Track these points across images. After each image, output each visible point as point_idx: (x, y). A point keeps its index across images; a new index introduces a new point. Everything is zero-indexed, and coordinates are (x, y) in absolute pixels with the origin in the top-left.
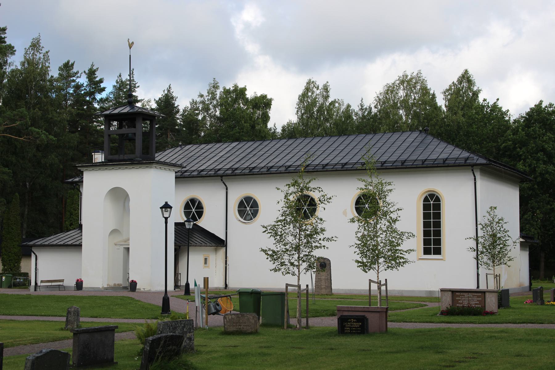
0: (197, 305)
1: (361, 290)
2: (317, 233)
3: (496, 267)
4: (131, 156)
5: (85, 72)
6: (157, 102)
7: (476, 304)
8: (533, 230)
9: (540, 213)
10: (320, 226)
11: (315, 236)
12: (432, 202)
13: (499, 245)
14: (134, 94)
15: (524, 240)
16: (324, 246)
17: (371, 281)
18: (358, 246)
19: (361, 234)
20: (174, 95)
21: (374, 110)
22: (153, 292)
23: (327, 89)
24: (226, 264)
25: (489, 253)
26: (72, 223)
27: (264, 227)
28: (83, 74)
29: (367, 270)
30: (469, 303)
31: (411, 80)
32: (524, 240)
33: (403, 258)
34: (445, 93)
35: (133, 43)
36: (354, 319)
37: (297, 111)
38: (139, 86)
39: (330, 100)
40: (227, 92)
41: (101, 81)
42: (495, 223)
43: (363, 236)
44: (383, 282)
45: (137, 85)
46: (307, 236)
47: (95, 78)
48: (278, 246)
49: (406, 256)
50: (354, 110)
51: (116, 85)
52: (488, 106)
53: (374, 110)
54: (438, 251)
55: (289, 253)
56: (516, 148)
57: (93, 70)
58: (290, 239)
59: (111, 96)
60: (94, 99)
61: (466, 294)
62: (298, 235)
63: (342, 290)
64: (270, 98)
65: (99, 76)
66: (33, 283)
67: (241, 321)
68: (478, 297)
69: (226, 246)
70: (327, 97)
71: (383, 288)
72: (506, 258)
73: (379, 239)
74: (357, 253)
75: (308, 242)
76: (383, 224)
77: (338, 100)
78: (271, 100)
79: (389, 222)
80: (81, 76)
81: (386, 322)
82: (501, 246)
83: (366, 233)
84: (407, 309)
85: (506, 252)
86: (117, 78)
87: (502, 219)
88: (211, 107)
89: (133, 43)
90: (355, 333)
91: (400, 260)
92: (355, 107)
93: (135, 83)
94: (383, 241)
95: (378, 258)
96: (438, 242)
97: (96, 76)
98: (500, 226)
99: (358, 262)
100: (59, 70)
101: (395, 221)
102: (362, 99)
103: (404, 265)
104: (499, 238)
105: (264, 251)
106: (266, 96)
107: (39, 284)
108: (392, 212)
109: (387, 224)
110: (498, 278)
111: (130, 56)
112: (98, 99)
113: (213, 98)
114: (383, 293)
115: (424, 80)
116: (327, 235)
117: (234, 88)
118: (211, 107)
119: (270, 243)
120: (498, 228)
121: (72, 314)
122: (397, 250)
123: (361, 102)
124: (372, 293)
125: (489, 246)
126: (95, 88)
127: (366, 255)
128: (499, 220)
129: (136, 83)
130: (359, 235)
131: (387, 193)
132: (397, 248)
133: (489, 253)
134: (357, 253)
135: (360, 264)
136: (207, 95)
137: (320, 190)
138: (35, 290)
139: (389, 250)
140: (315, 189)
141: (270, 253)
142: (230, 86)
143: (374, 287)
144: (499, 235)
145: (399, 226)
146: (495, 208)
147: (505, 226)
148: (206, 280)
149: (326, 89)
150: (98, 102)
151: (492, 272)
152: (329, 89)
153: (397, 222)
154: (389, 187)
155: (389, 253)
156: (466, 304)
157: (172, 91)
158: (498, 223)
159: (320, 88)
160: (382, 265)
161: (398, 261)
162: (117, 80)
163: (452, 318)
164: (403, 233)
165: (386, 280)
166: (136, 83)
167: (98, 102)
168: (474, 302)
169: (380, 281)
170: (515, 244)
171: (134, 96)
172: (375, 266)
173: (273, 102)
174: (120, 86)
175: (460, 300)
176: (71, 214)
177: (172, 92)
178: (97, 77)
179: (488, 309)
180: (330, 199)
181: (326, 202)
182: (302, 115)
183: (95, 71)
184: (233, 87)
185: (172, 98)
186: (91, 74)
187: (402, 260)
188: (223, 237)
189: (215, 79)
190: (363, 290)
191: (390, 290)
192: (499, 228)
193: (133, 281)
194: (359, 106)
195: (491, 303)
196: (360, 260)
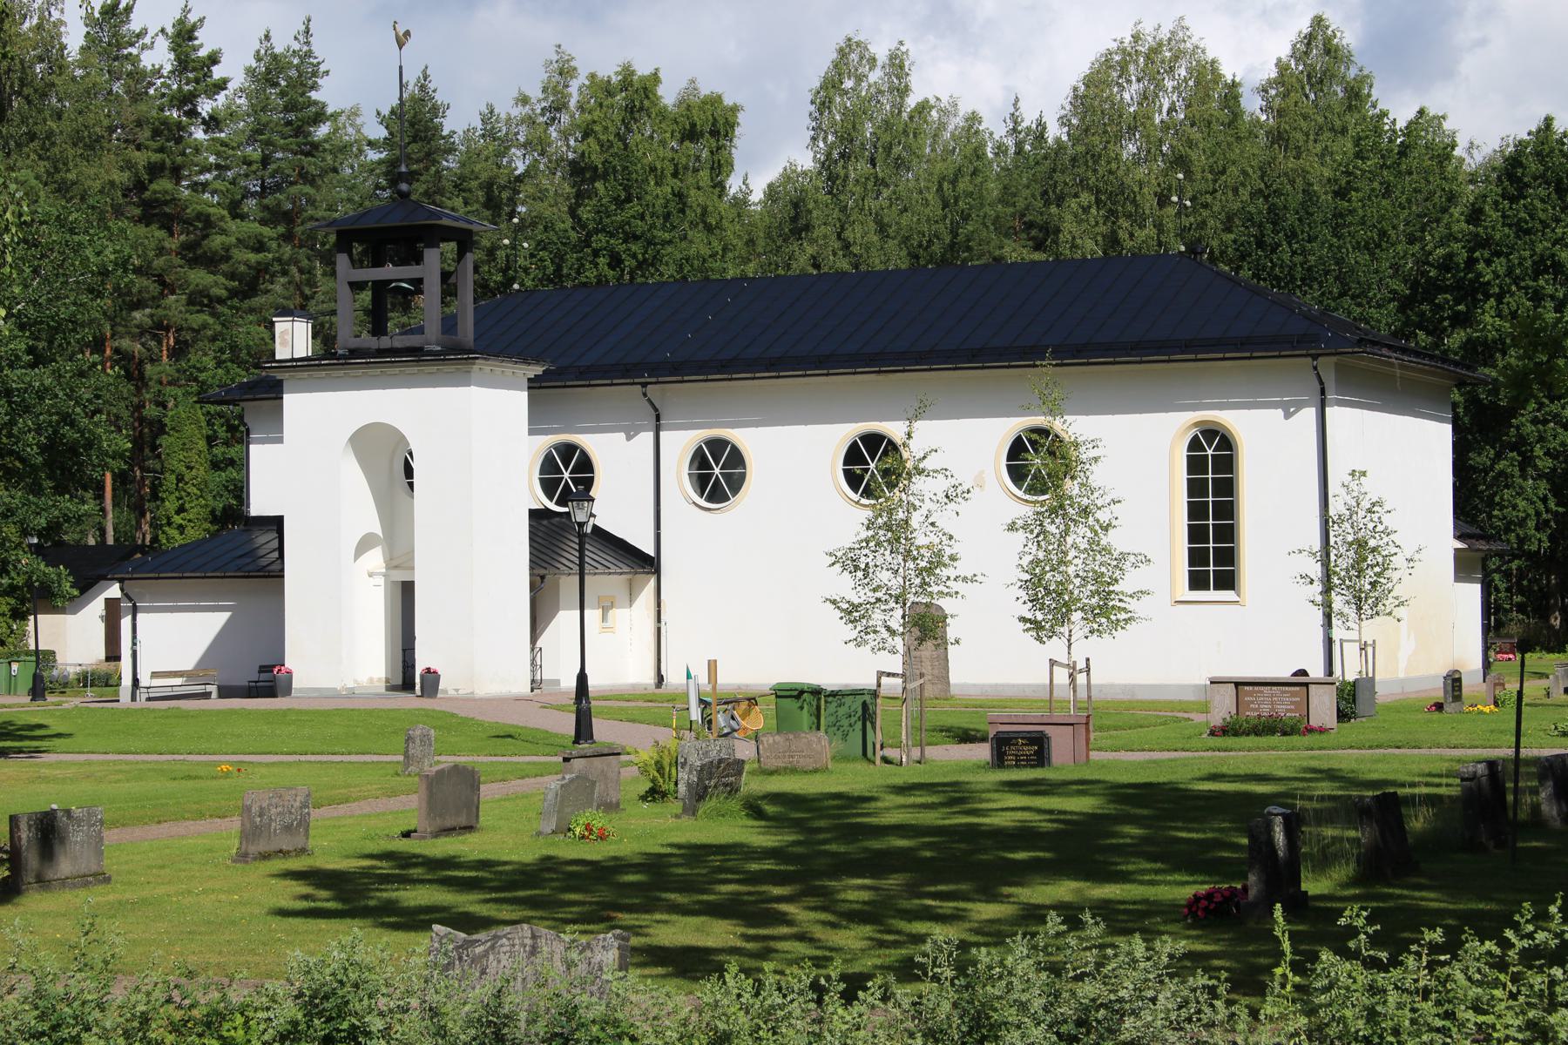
0: (694, 718)
1: (1024, 685)
2: (940, 564)
3: (1364, 623)
4: (413, 341)
5: (163, 31)
6: (384, 121)
7: (1288, 710)
8: (1522, 504)
9: (1545, 454)
10: (948, 551)
11: (937, 571)
12: (1210, 452)
13: (1372, 566)
14: (314, 95)
15: (1465, 546)
16: (957, 593)
17: (1053, 663)
18: (1025, 585)
19: (1031, 558)
20: (439, 98)
21: (1054, 132)
22: (481, 699)
23: (901, 67)
24: (659, 620)
25: (1348, 587)
26: (183, 505)
27: (831, 554)
28: (161, 37)
29: (1045, 639)
30: (1273, 709)
31: (1155, 50)
32: (1465, 546)
33: (1124, 609)
34: (1267, 92)
35: (407, 34)
36: (1022, 738)
37: (814, 139)
38: (327, 73)
39: (912, 101)
40: (602, 89)
41: (214, 59)
42: (1361, 513)
43: (1036, 562)
44: (1081, 665)
45: (322, 68)
46: (920, 572)
47: (196, 49)
48: (862, 592)
49: (1132, 604)
50: (991, 134)
51: (254, 65)
52: (1394, 131)
53: (1054, 132)
54: (1227, 581)
55: (883, 607)
56: (1477, 260)
57: (188, 26)
58: (884, 576)
59: (238, 101)
60: (193, 113)
61: (1266, 689)
62: (901, 570)
63: (975, 685)
64: (731, 104)
65: (206, 42)
66: (127, 681)
67: (793, 748)
68: (1293, 694)
69: (657, 572)
70: (904, 91)
71: (1081, 679)
72: (1391, 600)
73: (1071, 570)
74: (1021, 601)
75: (924, 584)
76: (1079, 536)
77: (938, 99)
78: (735, 109)
79: (1092, 529)
80: (153, 43)
81: (1088, 750)
82: (1377, 569)
83: (1041, 555)
84: (1141, 727)
85: (1390, 585)
86: (257, 46)
87: (1378, 503)
88: (554, 134)
89: (407, 34)
90: (1025, 766)
91: (1119, 616)
92: (995, 128)
93: (315, 61)
94: (1081, 574)
95: (1069, 610)
96: (1228, 557)
97: (196, 42)
98: (1376, 519)
99: (1023, 619)
100: (87, 25)
101: (1106, 528)
102: (1017, 100)
103: (1128, 626)
104: (1374, 550)
105: (834, 602)
106: (719, 99)
107: (145, 681)
108: (1099, 508)
109: (1089, 534)
110: (1370, 650)
111: (401, 67)
112: (204, 114)
113: (558, 107)
114: (1082, 694)
115: (1197, 47)
116: (962, 568)
117: (620, 78)
118: (554, 134)
119: (846, 587)
120: (1371, 526)
121: (418, 741)
122: (1110, 593)
123: (1012, 110)
124: (1055, 694)
125: (1347, 570)
126: (197, 81)
127: (1043, 604)
128: (1374, 505)
129: (319, 63)
130: (1027, 560)
131: (1088, 466)
132: (1111, 588)
133: (1348, 587)
134: (1021, 601)
135: (1028, 625)
136: (541, 96)
137: (948, 473)
138: (133, 698)
139: (1093, 595)
140: (937, 471)
141: (845, 606)
142: (609, 70)
143: (1061, 676)
144: (1372, 543)
145: (1112, 539)
146: (1364, 474)
147: (1386, 519)
148: (712, 666)
149: (897, 65)
150: (204, 122)
151: (1353, 635)
152: (907, 64)
153: (1111, 531)
154: (1092, 453)
155: (1094, 601)
156: (1265, 710)
157: (432, 86)
158: (1369, 511)
159: (879, 63)
160: (1078, 627)
161: (1113, 618)
162: (258, 52)
163: (1230, 741)
164: (1123, 557)
165: (1088, 660)
166: (319, 63)
167: (204, 122)
168: (1284, 705)
169: (1075, 663)
170: (1411, 564)
171: (316, 103)
172: (1062, 630)
173: (741, 117)
174: (268, 71)
175: (1252, 702)
176: (180, 478)
177: (434, 91)
178: (201, 46)
179: (1314, 722)
180: (968, 492)
181: (960, 500)
182: (831, 147)
183: (194, 28)
184: (617, 73)
185: (435, 110)
186: (184, 35)
187: (1123, 616)
188: (650, 550)
189: (559, 46)
190: (1029, 686)
191: (1097, 686)
192: (1372, 525)
193: (428, 669)
194: (1008, 120)
195: (1323, 708)
196: (1029, 616)
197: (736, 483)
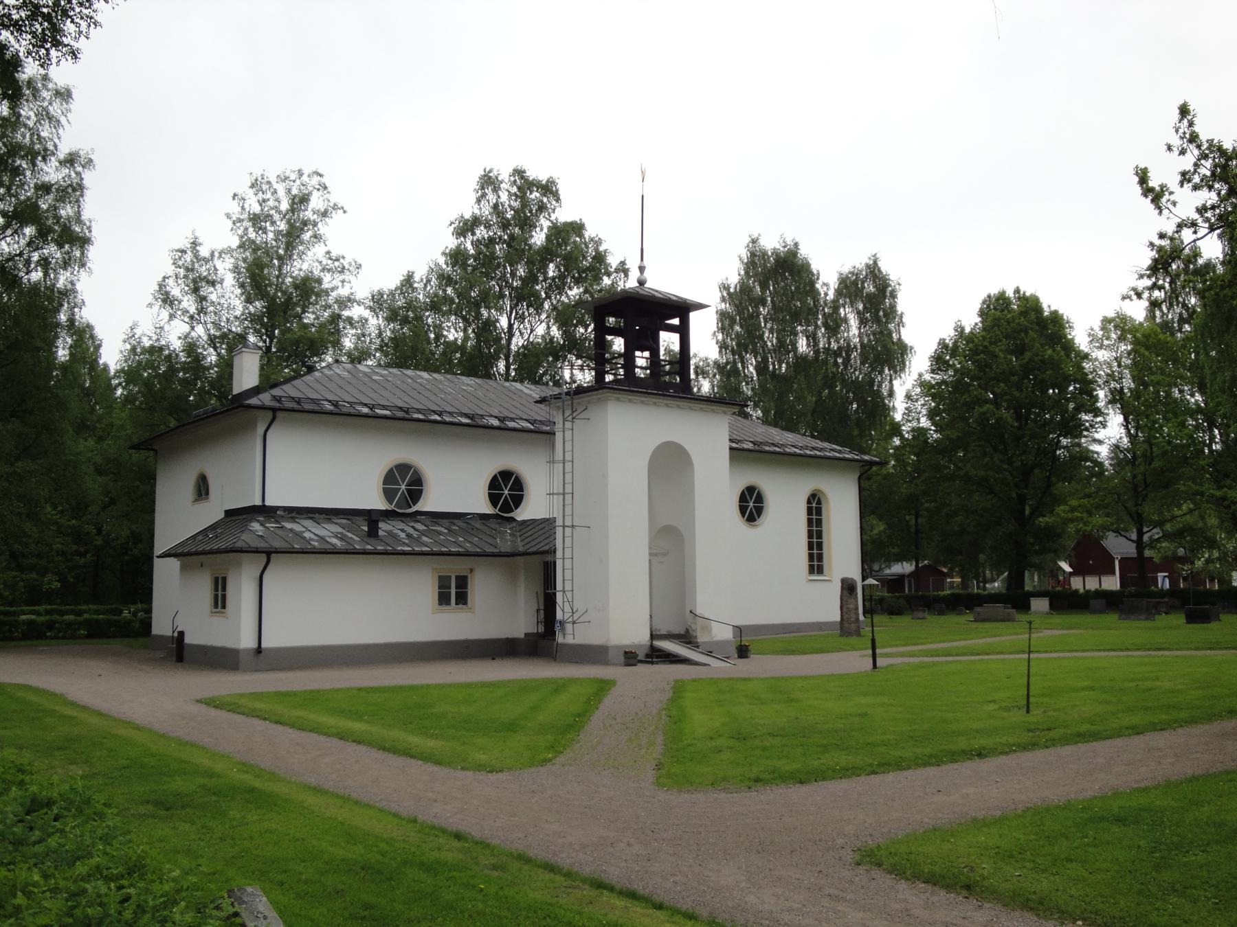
111: (643, 196)
197: (759, 511)
